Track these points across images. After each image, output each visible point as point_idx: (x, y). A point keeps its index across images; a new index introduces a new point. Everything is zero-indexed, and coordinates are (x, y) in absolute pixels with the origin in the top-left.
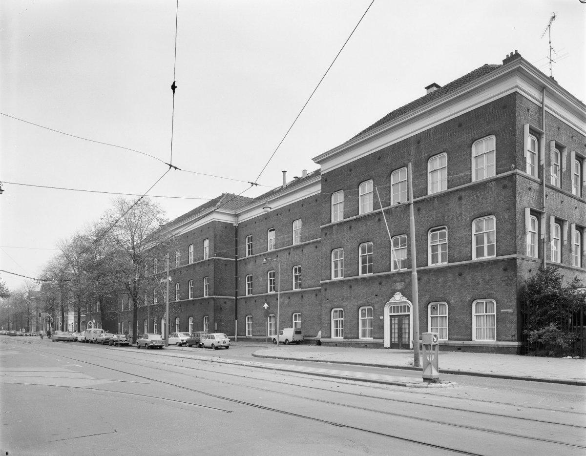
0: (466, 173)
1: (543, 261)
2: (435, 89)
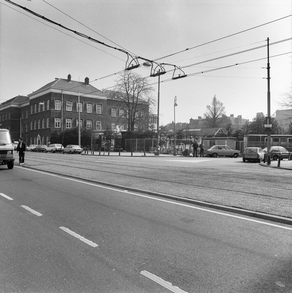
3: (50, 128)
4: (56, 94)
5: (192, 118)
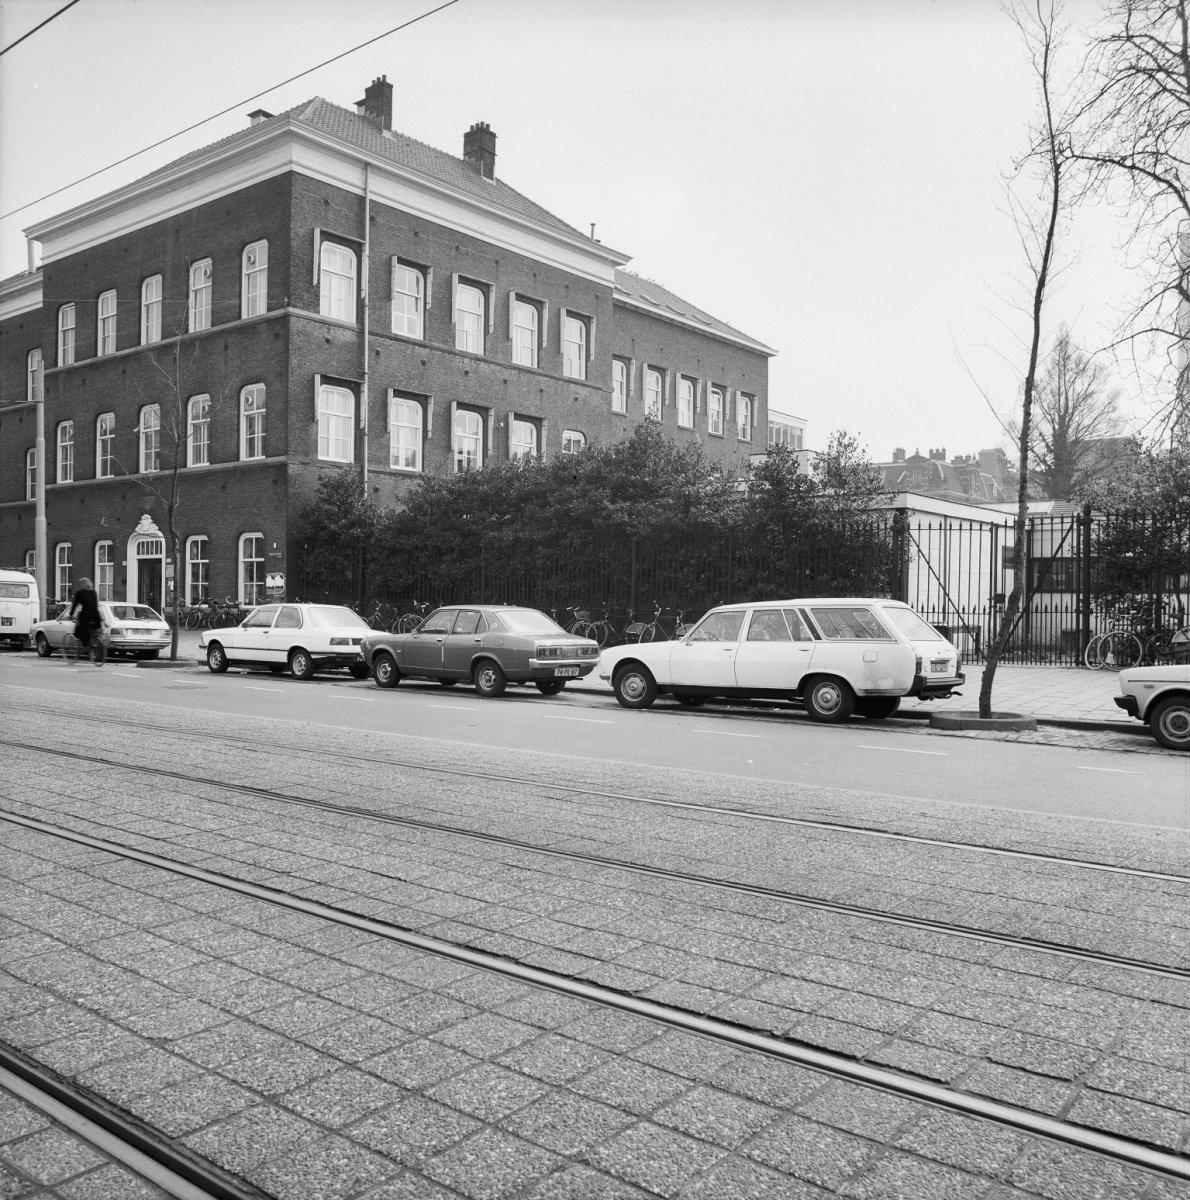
0: (235, 301)
1: (362, 467)
2: (263, 119)
3: (283, 466)
4: (327, 196)
5: (917, 453)
